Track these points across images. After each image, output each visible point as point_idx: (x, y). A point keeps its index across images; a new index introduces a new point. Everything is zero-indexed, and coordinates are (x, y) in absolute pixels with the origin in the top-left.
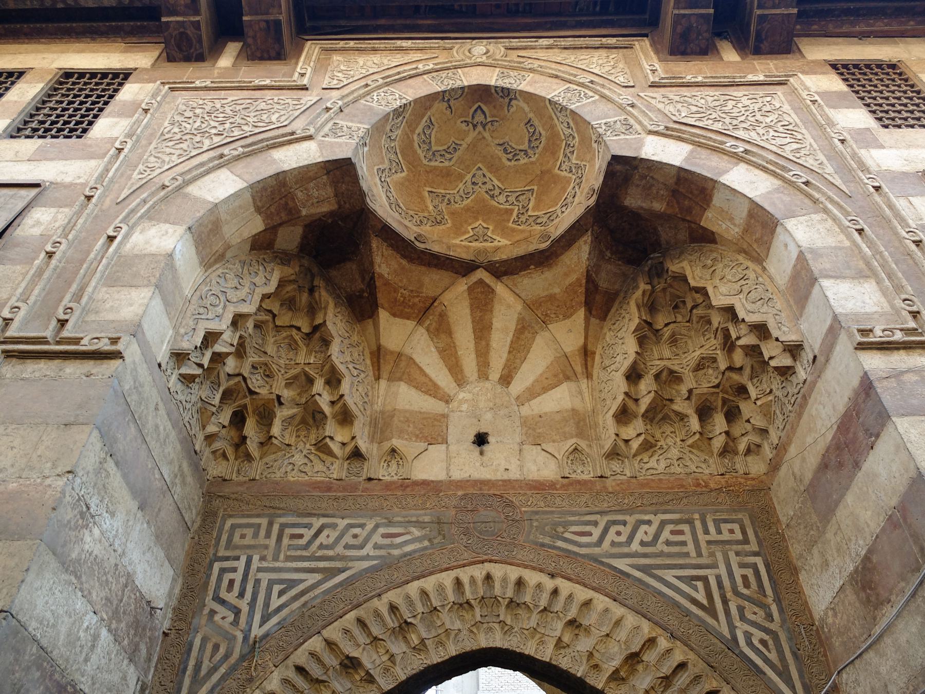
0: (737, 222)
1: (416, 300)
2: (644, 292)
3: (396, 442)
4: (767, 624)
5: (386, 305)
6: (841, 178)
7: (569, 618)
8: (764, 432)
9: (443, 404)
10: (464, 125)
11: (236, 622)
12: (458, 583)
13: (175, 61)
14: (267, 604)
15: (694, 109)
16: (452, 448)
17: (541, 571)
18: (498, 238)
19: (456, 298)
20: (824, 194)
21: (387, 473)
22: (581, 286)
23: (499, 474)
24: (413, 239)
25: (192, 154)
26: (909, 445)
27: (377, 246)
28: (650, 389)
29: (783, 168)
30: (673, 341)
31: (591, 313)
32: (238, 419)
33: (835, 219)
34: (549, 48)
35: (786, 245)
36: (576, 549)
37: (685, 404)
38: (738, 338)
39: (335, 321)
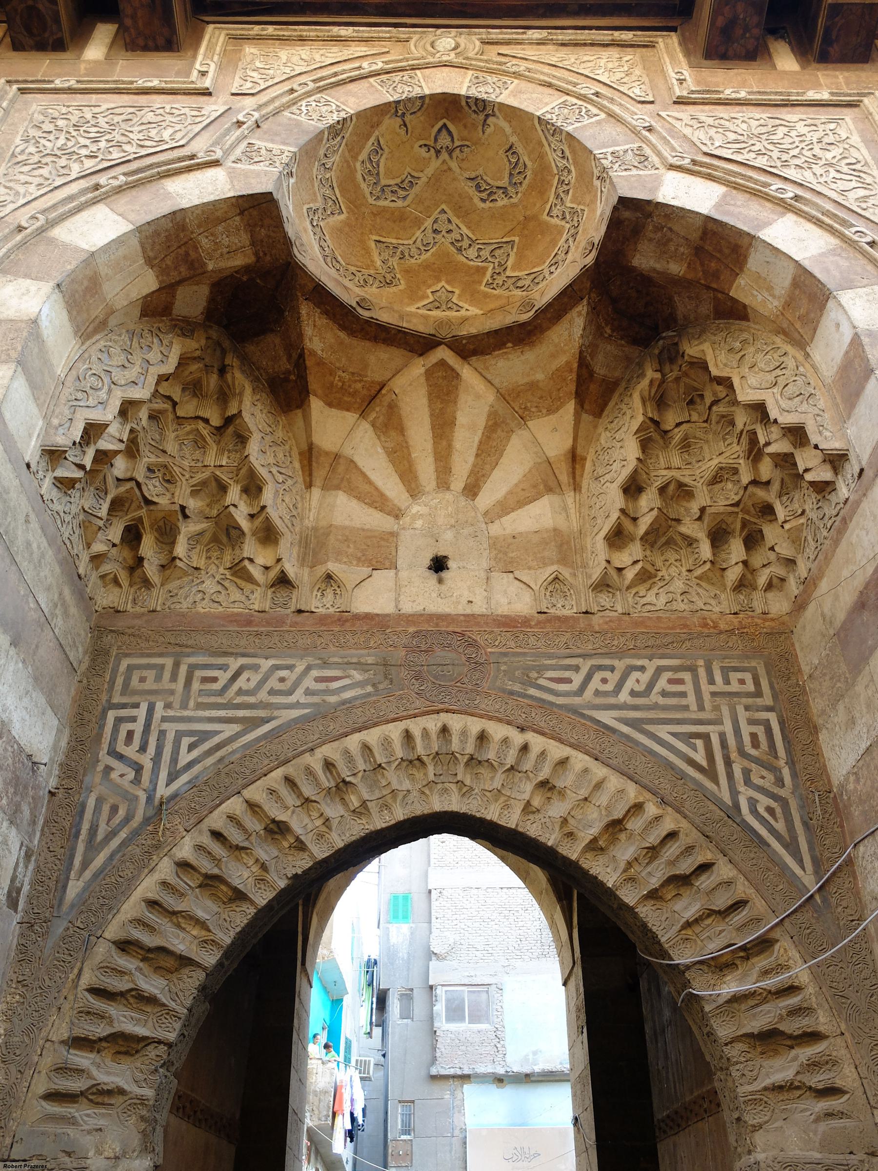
1: (359, 386)
2: (652, 382)
3: (332, 566)
5: (320, 392)
8: (791, 562)
9: (391, 519)
11: (137, 781)
12: (408, 736)
14: (174, 760)
15: (732, 136)
16: (403, 574)
17: (509, 723)
18: (466, 306)
19: (410, 384)
21: (322, 604)
22: (571, 371)
23: (460, 607)
24: (354, 304)
29: (844, 223)
30: (686, 445)
32: (132, 536)
34: (541, 43)
35: (838, 325)
38: (768, 444)
39: (254, 411)
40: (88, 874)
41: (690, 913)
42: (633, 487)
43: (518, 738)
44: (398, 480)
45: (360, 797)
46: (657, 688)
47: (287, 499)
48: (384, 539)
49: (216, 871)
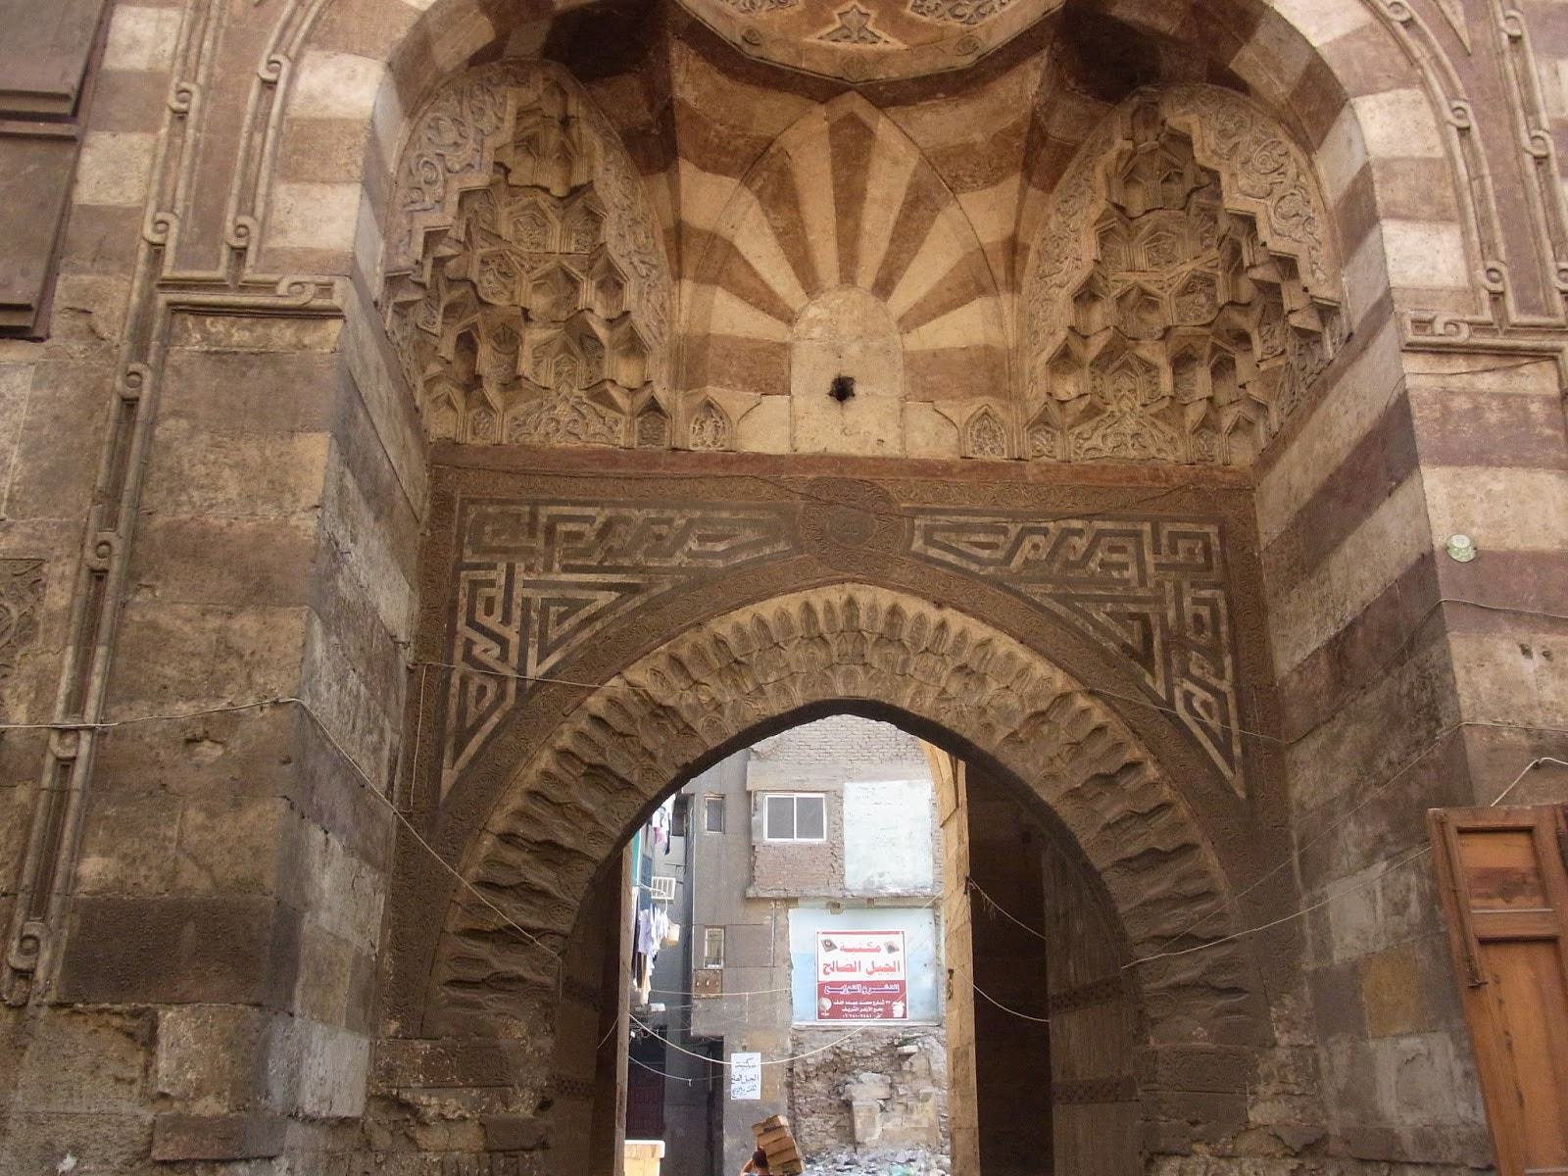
0: (1287, 78)
1: (741, 142)
2: (1121, 154)
3: (713, 392)
4: (1213, 681)
5: (691, 153)
7: (958, 664)
8: (1262, 407)
9: (782, 326)
11: (504, 657)
12: (808, 608)
14: (543, 634)
16: (800, 402)
17: (925, 597)
18: (885, 36)
21: (698, 438)
23: (868, 448)
24: (739, 40)
26: (1430, 510)
27: (679, 53)
28: (1109, 323)
31: (1029, 179)
32: (467, 343)
33: (1433, 103)
35: (1350, 141)
36: (974, 567)
37: (1157, 348)
38: (1253, 266)
39: (609, 178)
41: (1110, 816)
42: (1086, 295)
43: (934, 616)
44: (791, 273)
45: (755, 681)
47: (652, 298)
48: (774, 354)
49: (598, 760)
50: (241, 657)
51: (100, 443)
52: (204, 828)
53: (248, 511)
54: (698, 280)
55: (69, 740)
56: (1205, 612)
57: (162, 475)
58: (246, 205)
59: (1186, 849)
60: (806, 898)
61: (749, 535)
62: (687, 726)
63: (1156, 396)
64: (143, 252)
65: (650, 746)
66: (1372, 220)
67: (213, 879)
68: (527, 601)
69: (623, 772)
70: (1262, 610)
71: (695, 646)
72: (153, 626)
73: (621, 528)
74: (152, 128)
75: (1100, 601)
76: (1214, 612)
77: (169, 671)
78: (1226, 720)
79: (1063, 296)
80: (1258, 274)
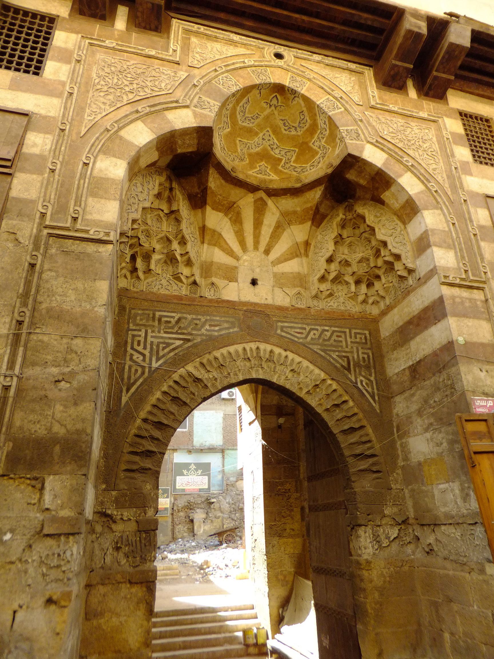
1: (225, 202)
2: (342, 219)
4: (369, 377)
5: (210, 204)
6: (451, 191)
9: (235, 261)
10: (265, 104)
11: (144, 360)
12: (244, 349)
13: (85, 15)
15: (391, 130)
16: (241, 285)
17: (281, 347)
18: (273, 175)
19: (247, 203)
20: (442, 199)
21: (209, 294)
22: (312, 210)
25: (118, 106)
29: (427, 180)
30: (350, 245)
32: (133, 258)
33: (444, 215)
34: (319, 62)
35: (420, 223)
36: (296, 339)
38: (385, 256)
40: (130, 394)
41: (339, 417)
43: (284, 353)
46: (333, 338)
49: (176, 395)
50: (76, 353)
51: (21, 278)
52: (63, 412)
53: (79, 304)
54: (209, 244)
55: (8, 379)
56: (366, 356)
57: (45, 290)
58: (78, 201)
59: (362, 427)
60: (180, 449)
61: (226, 325)
62: (206, 385)
63: (349, 292)
64: (38, 215)
65: (193, 391)
66: (429, 246)
67: (67, 430)
68: (152, 343)
69: (184, 399)
70: (382, 356)
71: (208, 359)
72: (42, 341)
73: (184, 321)
74: (41, 173)
75: (334, 351)
76: (369, 357)
77: (49, 357)
78: (373, 389)
79: (323, 260)
80: (386, 259)
